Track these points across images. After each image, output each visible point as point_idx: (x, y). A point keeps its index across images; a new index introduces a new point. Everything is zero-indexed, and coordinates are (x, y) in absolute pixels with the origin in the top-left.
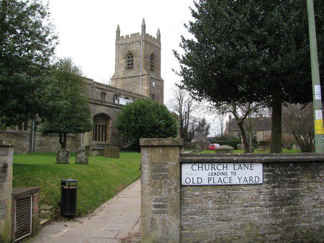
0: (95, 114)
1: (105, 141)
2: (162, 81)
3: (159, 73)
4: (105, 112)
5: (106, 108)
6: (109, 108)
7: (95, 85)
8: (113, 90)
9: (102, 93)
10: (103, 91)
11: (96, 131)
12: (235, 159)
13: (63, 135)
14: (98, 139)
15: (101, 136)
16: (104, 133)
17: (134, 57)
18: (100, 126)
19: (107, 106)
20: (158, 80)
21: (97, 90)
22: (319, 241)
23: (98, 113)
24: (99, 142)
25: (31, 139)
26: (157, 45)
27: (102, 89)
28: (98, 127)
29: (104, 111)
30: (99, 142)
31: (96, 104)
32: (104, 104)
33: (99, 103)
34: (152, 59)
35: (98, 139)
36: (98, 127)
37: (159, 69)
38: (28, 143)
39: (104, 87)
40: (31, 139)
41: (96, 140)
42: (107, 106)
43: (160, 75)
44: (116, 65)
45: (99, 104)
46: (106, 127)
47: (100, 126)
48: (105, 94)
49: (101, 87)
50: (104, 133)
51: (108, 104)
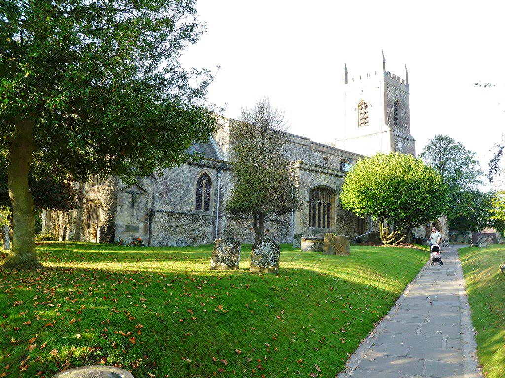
0: (313, 186)
1: (328, 227)
2: (412, 140)
3: (407, 130)
4: (328, 184)
5: (329, 177)
6: (334, 178)
7: (313, 146)
8: (340, 153)
9: (323, 158)
10: (326, 154)
11: (314, 214)
12: (203, 163)
13: (260, 216)
14: (317, 224)
15: (317, 216)
16: (326, 216)
17: (369, 106)
18: (319, 204)
19: (330, 174)
20: (408, 139)
21: (316, 153)
22: (437, 252)
23: (316, 185)
24: (319, 230)
25: (214, 224)
26: (404, 88)
27: (324, 152)
28: (317, 206)
29: (325, 183)
30: (319, 230)
31: (313, 171)
32: (325, 170)
33: (318, 169)
34: (396, 109)
35: (317, 224)
36: (317, 206)
37: (407, 122)
38: (210, 229)
39: (325, 149)
40: (214, 224)
41: (314, 226)
42: (330, 174)
43: (409, 131)
44: (324, 146)
45: (317, 171)
46: (329, 206)
47: (319, 204)
48: (328, 160)
49: (321, 149)
50: (326, 216)
51: (332, 172)
